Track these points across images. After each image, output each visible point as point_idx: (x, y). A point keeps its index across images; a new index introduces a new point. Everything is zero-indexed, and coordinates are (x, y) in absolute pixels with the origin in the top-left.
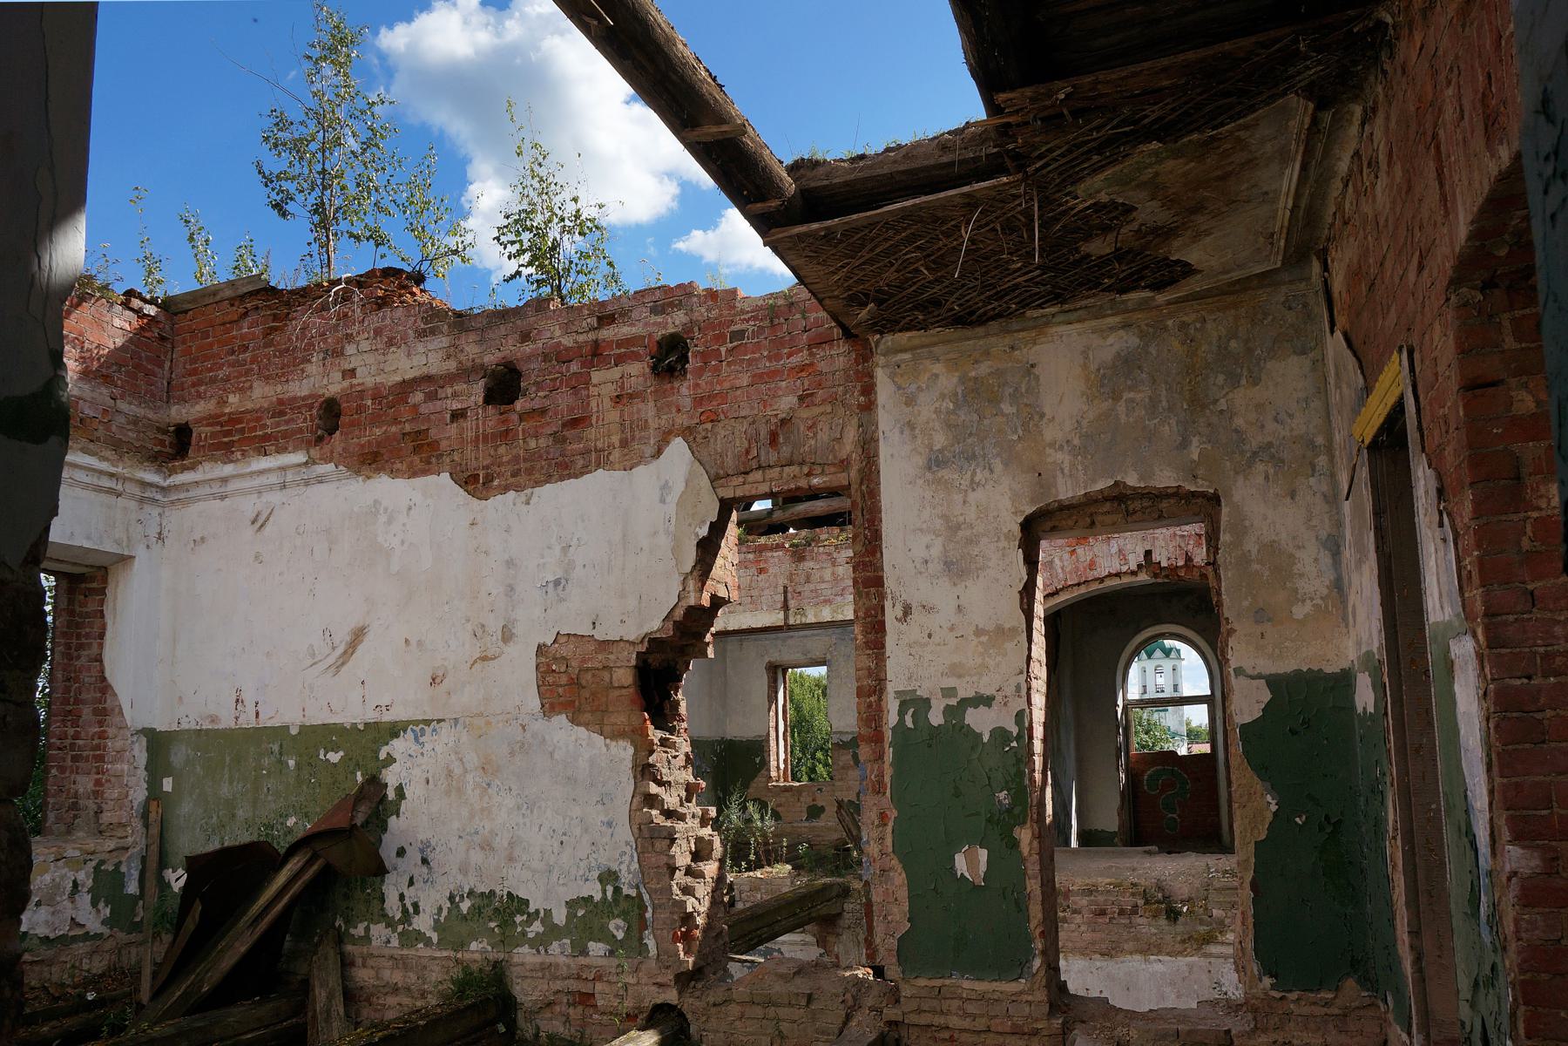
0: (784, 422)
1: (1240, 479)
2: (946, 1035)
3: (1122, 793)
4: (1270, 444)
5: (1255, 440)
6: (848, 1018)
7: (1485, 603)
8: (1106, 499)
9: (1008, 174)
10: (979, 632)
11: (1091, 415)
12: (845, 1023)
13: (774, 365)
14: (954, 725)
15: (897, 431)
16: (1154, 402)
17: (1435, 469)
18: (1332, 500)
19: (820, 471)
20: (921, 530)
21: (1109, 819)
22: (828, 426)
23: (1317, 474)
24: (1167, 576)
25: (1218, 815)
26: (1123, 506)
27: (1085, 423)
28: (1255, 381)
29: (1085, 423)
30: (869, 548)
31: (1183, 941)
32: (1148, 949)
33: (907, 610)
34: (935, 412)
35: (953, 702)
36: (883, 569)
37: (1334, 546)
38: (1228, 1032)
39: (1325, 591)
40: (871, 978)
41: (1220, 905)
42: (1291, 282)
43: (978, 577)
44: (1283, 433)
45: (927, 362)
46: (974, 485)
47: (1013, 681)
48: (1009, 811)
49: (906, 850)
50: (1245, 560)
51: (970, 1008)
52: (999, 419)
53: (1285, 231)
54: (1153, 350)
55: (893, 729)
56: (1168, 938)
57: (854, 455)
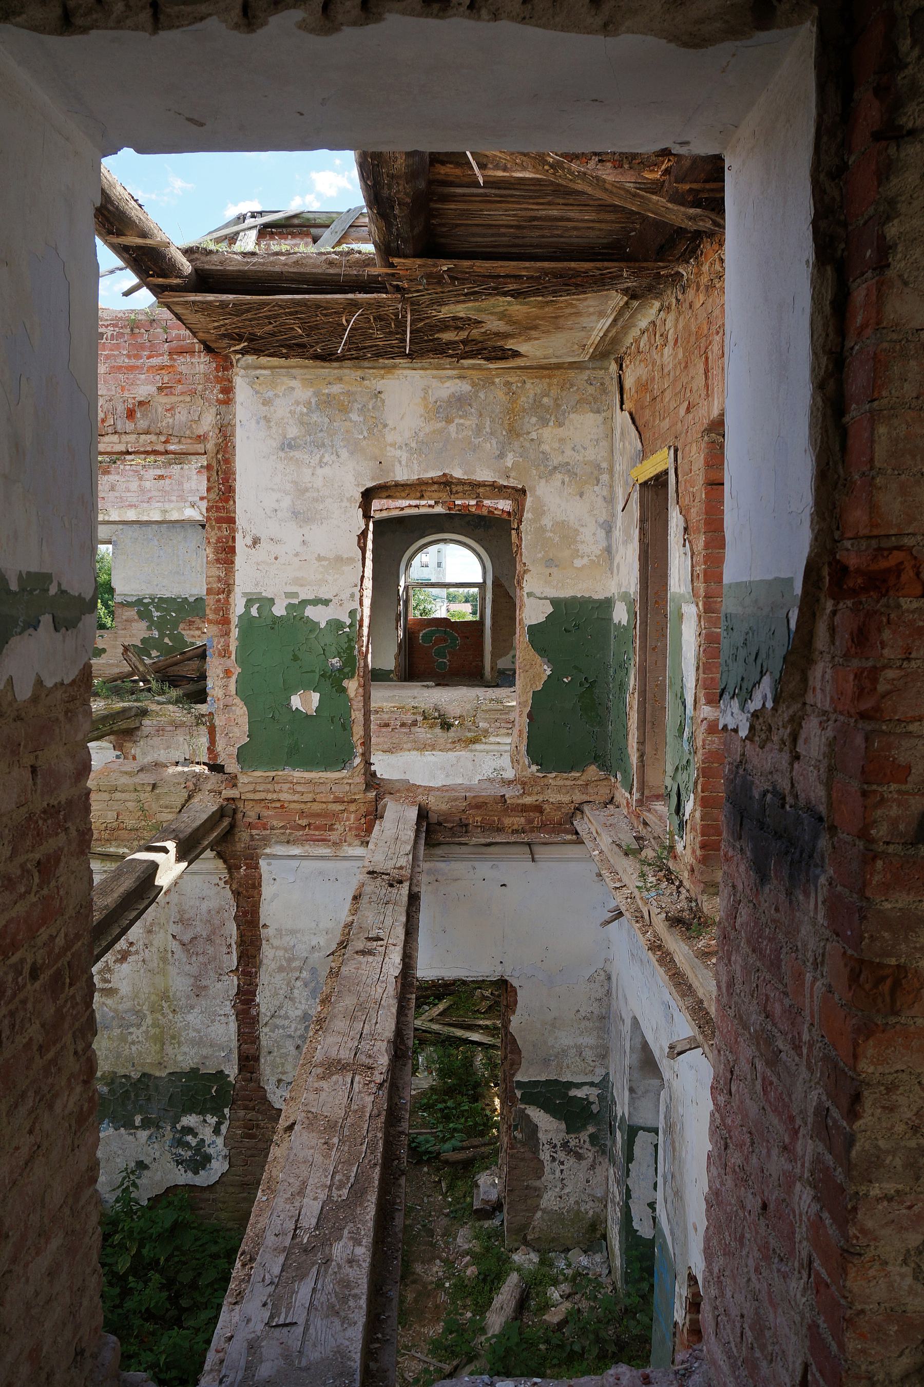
0: (141, 403)
1: (543, 481)
2: (278, 805)
3: (400, 646)
4: (567, 464)
5: (556, 460)
6: (190, 797)
7: (705, 591)
8: (434, 483)
9: (386, 293)
10: (320, 558)
11: (427, 430)
12: (187, 801)
13: (133, 362)
14: (295, 617)
15: (253, 422)
16: (479, 429)
17: (684, 516)
18: (610, 500)
19: (177, 440)
20: (273, 490)
21: (389, 662)
22: (186, 411)
23: (600, 485)
24: (459, 510)
25: (482, 661)
26: (448, 488)
27: (421, 434)
28: (561, 425)
29: (421, 434)
30: (223, 497)
31: (454, 742)
32: (422, 747)
33: (256, 541)
34: (290, 412)
35: (296, 601)
36: (235, 512)
37: (608, 528)
38: (504, 796)
39: (599, 553)
40: (206, 772)
41: (485, 720)
42: (594, 369)
43: (322, 523)
44: (578, 458)
45: (285, 379)
46: (321, 464)
47: (349, 592)
48: (340, 670)
49: (246, 692)
50: (542, 529)
51: (299, 788)
52: (348, 423)
53: (594, 346)
54: (482, 395)
55: (240, 617)
56: (442, 741)
57: (211, 434)
